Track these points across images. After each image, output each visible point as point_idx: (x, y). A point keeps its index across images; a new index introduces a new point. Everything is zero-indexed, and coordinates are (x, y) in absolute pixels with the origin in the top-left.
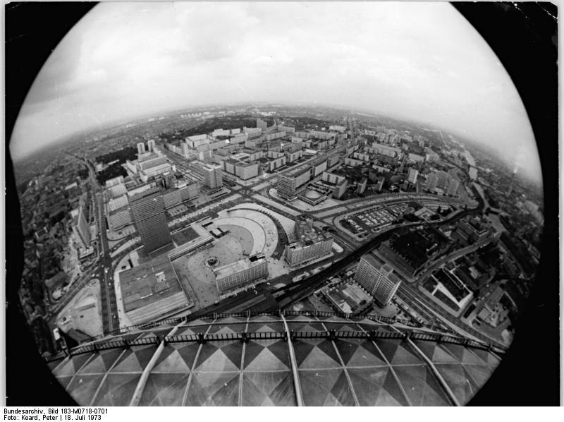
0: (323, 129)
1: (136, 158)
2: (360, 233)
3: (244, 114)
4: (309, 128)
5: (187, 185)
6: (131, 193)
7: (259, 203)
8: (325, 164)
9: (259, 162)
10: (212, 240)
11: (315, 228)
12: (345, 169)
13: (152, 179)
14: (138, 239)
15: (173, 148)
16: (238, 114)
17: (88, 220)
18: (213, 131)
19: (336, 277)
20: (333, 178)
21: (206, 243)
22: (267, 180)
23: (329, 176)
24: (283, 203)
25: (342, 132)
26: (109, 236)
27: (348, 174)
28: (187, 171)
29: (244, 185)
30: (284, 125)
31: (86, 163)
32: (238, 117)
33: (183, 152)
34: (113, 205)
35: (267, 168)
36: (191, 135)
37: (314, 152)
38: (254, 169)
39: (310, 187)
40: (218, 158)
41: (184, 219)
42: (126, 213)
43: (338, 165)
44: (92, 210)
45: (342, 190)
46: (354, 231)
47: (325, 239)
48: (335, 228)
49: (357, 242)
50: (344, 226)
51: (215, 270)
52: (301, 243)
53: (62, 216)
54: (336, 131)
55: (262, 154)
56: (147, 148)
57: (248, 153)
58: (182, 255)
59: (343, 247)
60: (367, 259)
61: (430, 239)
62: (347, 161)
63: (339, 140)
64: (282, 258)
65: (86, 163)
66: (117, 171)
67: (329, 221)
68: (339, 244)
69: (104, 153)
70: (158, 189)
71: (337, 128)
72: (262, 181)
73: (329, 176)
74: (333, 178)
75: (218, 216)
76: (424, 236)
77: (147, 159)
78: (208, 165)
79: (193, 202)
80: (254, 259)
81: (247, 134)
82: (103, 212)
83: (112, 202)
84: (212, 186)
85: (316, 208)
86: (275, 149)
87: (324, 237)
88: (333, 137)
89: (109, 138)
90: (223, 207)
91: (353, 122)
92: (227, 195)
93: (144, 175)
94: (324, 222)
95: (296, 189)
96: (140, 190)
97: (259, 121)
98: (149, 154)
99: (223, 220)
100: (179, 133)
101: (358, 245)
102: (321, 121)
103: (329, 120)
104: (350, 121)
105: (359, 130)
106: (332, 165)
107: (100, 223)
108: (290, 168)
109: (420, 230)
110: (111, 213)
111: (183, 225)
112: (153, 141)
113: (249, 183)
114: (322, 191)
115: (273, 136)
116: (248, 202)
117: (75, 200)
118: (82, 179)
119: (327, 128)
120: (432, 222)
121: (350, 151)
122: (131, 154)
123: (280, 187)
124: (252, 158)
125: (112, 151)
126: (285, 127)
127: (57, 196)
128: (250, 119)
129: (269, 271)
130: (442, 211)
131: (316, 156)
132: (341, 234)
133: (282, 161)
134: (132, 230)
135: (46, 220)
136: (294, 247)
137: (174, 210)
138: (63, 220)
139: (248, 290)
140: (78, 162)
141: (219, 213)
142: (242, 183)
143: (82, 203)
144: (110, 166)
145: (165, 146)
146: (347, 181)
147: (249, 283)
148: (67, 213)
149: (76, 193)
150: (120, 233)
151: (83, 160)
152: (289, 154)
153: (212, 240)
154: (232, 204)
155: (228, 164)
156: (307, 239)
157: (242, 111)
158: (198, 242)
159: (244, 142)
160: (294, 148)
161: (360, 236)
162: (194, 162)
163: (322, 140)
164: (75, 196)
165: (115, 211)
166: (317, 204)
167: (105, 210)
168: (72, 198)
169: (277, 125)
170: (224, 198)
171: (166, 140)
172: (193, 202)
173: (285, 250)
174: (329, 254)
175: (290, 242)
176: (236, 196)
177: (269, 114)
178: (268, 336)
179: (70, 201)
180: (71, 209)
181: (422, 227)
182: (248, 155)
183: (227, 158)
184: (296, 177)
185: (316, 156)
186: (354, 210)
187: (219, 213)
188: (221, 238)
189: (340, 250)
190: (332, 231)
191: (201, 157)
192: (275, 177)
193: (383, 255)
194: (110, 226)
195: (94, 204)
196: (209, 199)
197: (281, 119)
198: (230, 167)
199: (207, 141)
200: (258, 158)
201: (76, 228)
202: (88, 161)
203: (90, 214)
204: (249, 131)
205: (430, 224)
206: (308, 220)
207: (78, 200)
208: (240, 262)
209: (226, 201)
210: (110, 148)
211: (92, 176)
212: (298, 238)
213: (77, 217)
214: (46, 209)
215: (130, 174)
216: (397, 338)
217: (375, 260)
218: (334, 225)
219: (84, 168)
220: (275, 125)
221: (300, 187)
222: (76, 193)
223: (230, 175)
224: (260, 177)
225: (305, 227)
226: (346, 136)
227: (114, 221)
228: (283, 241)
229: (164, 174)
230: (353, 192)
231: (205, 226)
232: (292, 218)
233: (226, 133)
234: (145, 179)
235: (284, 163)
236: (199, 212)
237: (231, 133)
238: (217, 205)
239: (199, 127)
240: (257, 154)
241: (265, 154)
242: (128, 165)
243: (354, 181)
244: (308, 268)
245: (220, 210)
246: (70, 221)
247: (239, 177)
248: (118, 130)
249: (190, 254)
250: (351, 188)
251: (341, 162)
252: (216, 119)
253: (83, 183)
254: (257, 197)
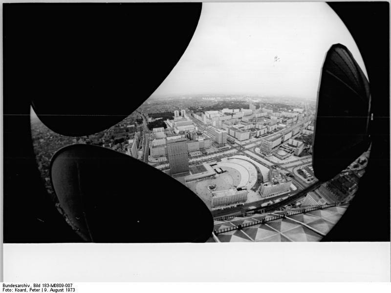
0: (290, 111)
1: (173, 119)
2: (309, 178)
3: (242, 100)
4: (281, 110)
5: (204, 140)
6: (169, 139)
7: (248, 156)
8: (291, 133)
9: (250, 130)
10: (215, 175)
11: (281, 174)
12: (303, 137)
13: (182, 133)
14: (167, 165)
15: (197, 116)
16: (238, 100)
17: (138, 147)
18: (222, 109)
19: (289, 205)
20: (295, 142)
21: (210, 176)
22: (255, 142)
23: (293, 141)
24: (263, 157)
25: (301, 112)
26: (149, 159)
27: (305, 140)
28: (205, 132)
29: (240, 144)
30: (266, 108)
31: (141, 115)
32: (238, 102)
33: (203, 120)
34: (155, 142)
35: (255, 135)
36: (209, 110)
37: (284, 126)
38: (246, 135)
39: (281, 148)
40: (225, 126)
41: (199, 159)
42: (163, 149)
43: (299, 134)
44: (142, 142)
45: (300, 150)
46: (305, 177)
47: (287, 181)
48: (293, 175)
49: (306, 184)
50: (299, 173)
51: (213, 192)
52: (272, 183)
53: (122, 140)
54: (298, 112)
55: (252, 126)
56: (180, 114)
57: (244, 124)
58: (193, 180)
59: (297, 187)
60: (312, 195)
61: (352, 181)
62: (304, 131)
63: (299, 118)
64: (257, 191)
65: (141, 115)
66: (161, 124)
67: (290, 170)
68: (295, 185)
69: (154, 112)
70: (186, 139)
71: (298, 110)
72: (251, 143)
73: (293, 141)
74: (295, 142)
75: (221, 161)
76: (348, 179)
77: (180, 120)
78: (219, 130)
79: (206, 150)
80: (239, 189)
81: (243, 113)
82: (148, 145)
83: (155, 141)
84: (220, 143)
85: (284, 161)
86: (260, 123)
87: (287, 180)
88: (296, 116)
89: (157, 104)
90: (225, 156)
91: (307, 106)
92: (227, 149)
93: (177, 129)
94: (288, 171)
95: (272, 149)
96: (175, 138)
97: (251, 106)
98: (181, 117)
99: (224, 164)
100: (201, 108)
101: (307, 186)
102: (289, 106)
103: (293, 105)
104: (305, 105)
105: (311, 111)
106: (295, 134)
107: (145, 150)
108: (270, 135)
109: (346, 175)
110: (153, 147)
111: (197, 163)
112: (184, 111)
113: (243, 143)
114: (288, 151)
115: (260, 115)
116: (241, 155)
117: (132, 134)
118: (138, 124)
119: (292, 110)
120: (354, 169)
121: (306, 125)
122: (170, 116)
123: (263, 147)
124: (246, 128)
125: (158, 112)
126: (266, 110)
127: (121, 129)
128: (245, 103)
129: (248, 197)
130: (361, 162)
131: (285, 129)
132: (297, 179)
133: (265, 131)
134: (165, 159)
135: (112, 140)
136: (267, 185)
137: (194, 153)
138: (122, 143)
139: (231, 207)
140: (137, 114)
141: (221, 159)
142: (239, 142)
143: (136, 137)
144: (157, 121)
145: (192, 115)
146: (303, 145)
147: (233, 204)
148: (126, 140)
149: (133, 130)
150: (156, 159)
151: (140, 113)
152: (269, 127)
153: (215, 175)
154: (231, 155)
155: (230, 130)
156: (276, 181)
157: (240, 99)
158: (205, 174)
159: (241, 118)
160: (272, 123)
161: (308, 180)
162: (210, 127)
163: (289, 118)
164: (132, 132)
165: (156, 147)
166: (284, 159)
167: (150, 145)
168: (131, 133)
169: (262, 108)
170: (226, 150)
171: (193, 111)
172: (206, 150)
173: (260, 187)
174: (288, 191)
175: (264, 181)
176: (234, 151)
177: (257, 101)
178: (226, 230)
179: (129, 134)
180: (129, 139)
181: (347, 173)
182: (244, 126)
183: (230, 126)
184: (272, 141)
185: (285, 129)
186: (307, 163)
187: (221, 159)
188: (221, 174)
189: (295, 188)
190: (291, 176)
191: (214, 124)
192: (259, 140)
193: (321, 193)
194: (151, 154)
195: (143, 139)
196: (217, 150)
197: (265, 104)
198: (232, 132)
199: (219, 115)
200: (249, 128)
201: (130, 150)
202: (143, 115)
203: (140, 144)
204: (244, 111)
205: (353, 171)
206: (277, 168)
207: (134, 135)
208: (230, 190)
209: (228, 152)
210: (158, 110)
211: (144, 124)
212: (269, 180)
213: (132, 144)
214: (113, 134)
215: (168, 127)
216: (279, 218)
217: (316, 196)
218: (294, 173)
219: (140, 118)
220: (260, 108)
221: (275, 148)
222: (133, 130)
223: (232, 137)
224: (250, 140)
225: (275, 173)
226: (303, 115)
227: (154, 152)
228: (260, 180)
229: (190, 131)
230: (306, 152)
231: (212, 166)
232: (268, 167)
233: (231, 111)
234: (177, 132)
235: (266, 132)
236: (209, 157)
237: (233, 111)
238: (221, 154)
239: (214, 106)
240: (249, 125)
241: (254, 126)
242: (168, 122)
243: (308, 144)
244: (272, 199)
245: (223, 158)
246: (127, 145)
247: (237, 139)
248: (163, 100)
249: (198, 180)
250: (305, 149)
251: (301, 132)
252: (224, 102)
253: (138, 126)
254: (247, 152)
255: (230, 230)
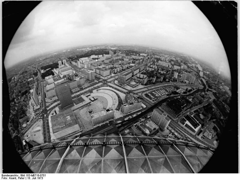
0: (138, 55)
1: (58, 67)
2: (153, 100)
3: (104, 49)
4: (132, 54)
5: (80, 79)
6: (56, 83)
7: (110, 86)
8: (138, 70)
9: (110, 69)
10: (90, 102)
11: (134, 97)
12: (147, 72)
13: (65, 76)
14: (59, 102)
15: (74, 63)
16: (101, 49)
17: (37, 94)
18: (91, 56)
19: (143, 118)
20: (142, 76)
21: (88, 104)
22: (114, 77)
23: (140, 75)
24: (120, 87)
25: (146, 56)
26: (46, 101)
27: (148, 74)
28: (80, 73)
29: (104, 79)
30: (121, 53)
31: (36, 69)
32: (101, 50)
33: (78, 65)
34: (48, 87)
35: (114, 72)
36: (81, 58)
37: (133, 65)
38: (108, 72)
39: (132, 80)
40: (93, 68)
41: (78, 93)
42: (54, 91)
43: (144, 71)
44: (39, 90)
45: (146, 81)
46: (151, 98)
47: (138, 102)
48: (142, 97)
49: (152, 103)
50: (146, 96)
51: (91, 115)
52: (128, 103)
53: (26, 92)
54: (143, 56)
55: (112, 66)
56: (62, 63)
57: (105, 65)
58: (77, 109)
59: (146, 106)
60: (156, 110)
61: (183, 102)
62: (148, 68)
63: (144, 60)
64: (120, 110)
65: (36, 69)
66: (50, 73)
67: (140, 94)
68: (144, 104)
69: (44, 65)
70: (67, 80)
71: (143, 54)
72: (112, 77)
73: (140, 75)
74: (142, 76)
75: (93, 92)
76: (180, 100)
77: (62, 68)
78: (89, 71)
79: (82, 86)
80: (108, 110)
81: (105, 57)
82: (44, 91)
83: (48, 86)
84: (90, 79)
85: (135, 89)
86: (117, 63)
87: (138, 101)
88: (142, 59)
89: (46, 59)
90: (95, 88)
91: (150, 52)
92: (97, 83)
93: (61, 74)
94: (138, 95)
95: (126, 81)
96: (60, 81)
97: (110, 52)
98: (63, 65)
99: (95, 94)
100: (76, 57)
101: (153, 105)
102: (136, 52)
103: (140, 51)
104: (149, 51)
105: (153, 55)
106: (141, 70)
107: (43, 95)
108: (123, 72)
109: (179, 98)
110: (47, 91)
111: (78, 96)
112: (65, 60)
113: (106, 78)
114: (137, 82)
115: (116, 58)
116: (106, 86)
117: (32, 85)
118: (35, 76)
119: (139, 55)
120: (184, 95)
121: (149, 64)
122: (56, 66)
123: (119, 80)
124: (107, 67)
125: (47, 64)
126: (121, 54)
127: (24, 84)
128: (106, 51)
129: (114, 115)
130: (188, 90)
131: (134, 67)
132: (145, 100)
133: (120, 69)
134: (56, 98)
135: (20, 94)
136: (125, 105)
137: (74, 89)
138: (27, 94)
139: (106, 123)
140: (33, 69)
141: (93, 91)
142: (103, 78)
143: (35, 87)
144: (47, 71)
145: (70, 62)
146: (148, 77)
147: (106, 121)
148: (28, 91)
149: (32, 82)
150: (51, 99)
151: (36, 68)
152: (123, 66)
153: (90, 102)
154: (99, 87)
155: (97, 70)
156: (131, 102)
157: (103, 47)
158: (84, 103)
159: (104, 61)
160: (125, 63)
161: (153, 101)
162: (83, 69)
163: (137, 60)
164: (32, 84)
165: (49, 90)
166: (135, 87)
167: (45, 90)
168: (31, 85)
169: (118, 53)
170: (95, 84)
171: (70, 60)
172: (82, 86)
173: (121, 107)
174: (140, 108)
175: (123, 103)
176: (100, 84)
177: (115, 49)
178: (114, 143)
179: (30, 86)
180: (30, 89)
181: (179, 97)
182: (105, 66)
183: (96, 67)
184: (126, 75)
185: (134, 67)
186: (151, 90)
187: (93, 91)
188: (94, 102)
189: (145, 106)
190: (141, 99)
191: (86, 67)
192: (117, 75)
193: (163, 109)
194: (47, 96)
195: (40, 87)
196: (89, 85)
197: (120, 51)
198: (98, 71)
199: (88, 60)
200: (110, 67)
201: (33, 97)
202: (38, 69)
203: (38, 91)
204: (106, 56)
205: (183, 96)
206: (131, 94)
207: (33, 86)
208: (102, 112)
209: (96, 86)
210: (47, 63)
211: (39, 75)
212: (127, 102)
213: (33, 92)
214: (19, 89)
215: (55, 74)
216: (169, 144)
217: (160, 111)
218: (142, 96)
219: (36, 71)
220: (117, 53)
221: (128, 80)
222: (32, 82)
223: (98, 75)
224: (111, 75)
225: (130, 97)
226: (147, 58)
227: (48, 94)
228: (120, 103)
229: (70, 74)
230: (150, 82)
231: (87, 96)
232: (124, 93)
233: (96, 57)
234: (62, 76)
235: (121, 69)
236: (85, 90)
237: (98, 57)
238: (92, 87)
239: (85, 54)
240: (109, 66)
241: (113, 66)
242: (55, 70)
243: (150, 77)
244: (131, 115)
245: (94, 90)
246: (30, 94)
247: (102, 75)
248: (50, 55)
249: (81, 108)
250: (149, 80)
251: (145, 69)
252: (92, 51)
253: (35, 78)
254: (109, 84)
255: (113, 144)
